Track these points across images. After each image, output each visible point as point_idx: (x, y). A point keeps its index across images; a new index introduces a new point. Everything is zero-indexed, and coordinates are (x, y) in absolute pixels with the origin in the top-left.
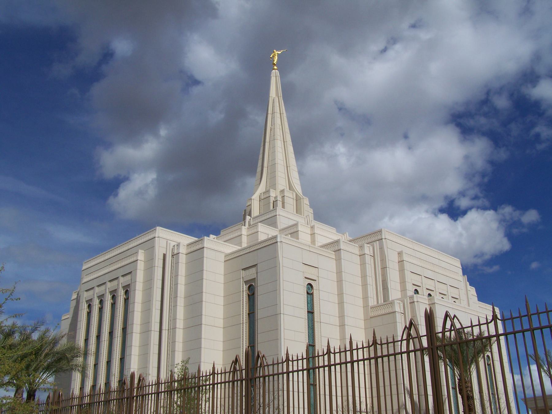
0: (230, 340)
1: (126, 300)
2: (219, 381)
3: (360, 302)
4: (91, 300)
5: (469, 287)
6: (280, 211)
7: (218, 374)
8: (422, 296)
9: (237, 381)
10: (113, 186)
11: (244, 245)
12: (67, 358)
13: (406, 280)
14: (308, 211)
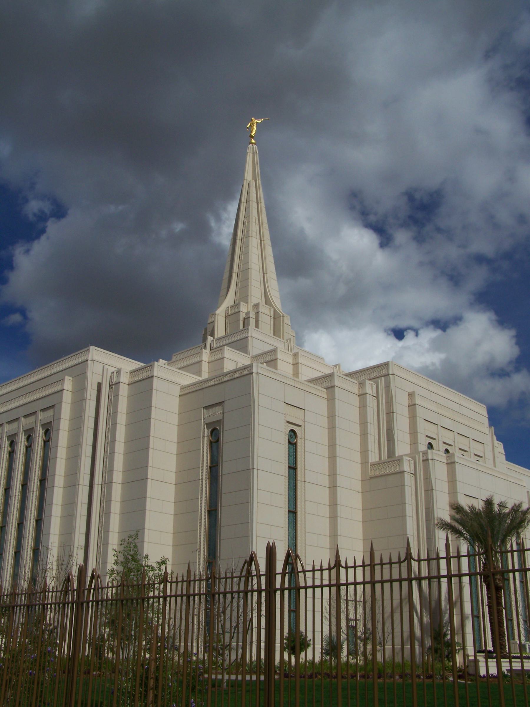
1: (46, 442)
3: (357, 457)
5: (496, 442)
6: (252, 331)
8: (438, 452)
11: (205, 375)
13: (418, 431)
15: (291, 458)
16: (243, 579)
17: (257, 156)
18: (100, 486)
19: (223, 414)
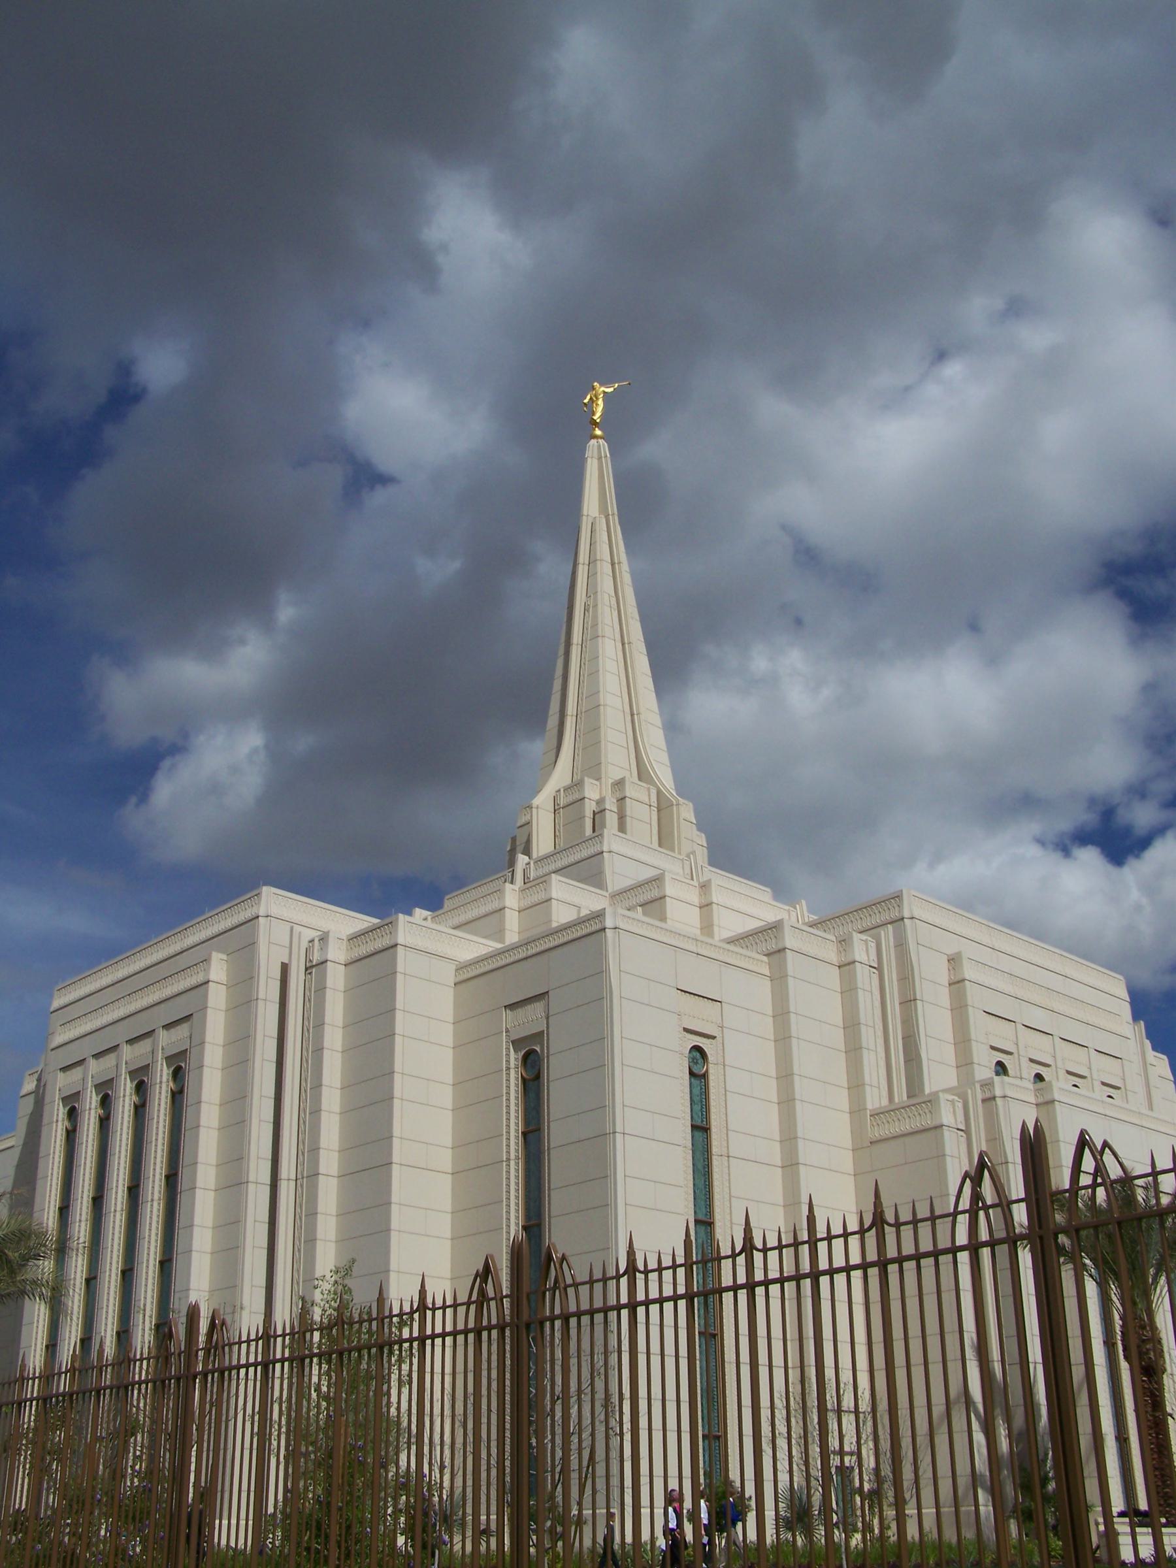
0: (471, 1209)
1: (177, 1096)
2: (438, 1330)
4: (76, 1096)
5: (1151, 1055)
6: (611, 840)
7: (434, 1309)
9: (489, 1328)
10: (139, 769)
11: (512, 936)
12: (8, 1261)
13: (973, 1037)
14: (692, 839)
15: (697, 1108)
16: (473, 1307)
18: (293, 1184)
19: (547, 1018)
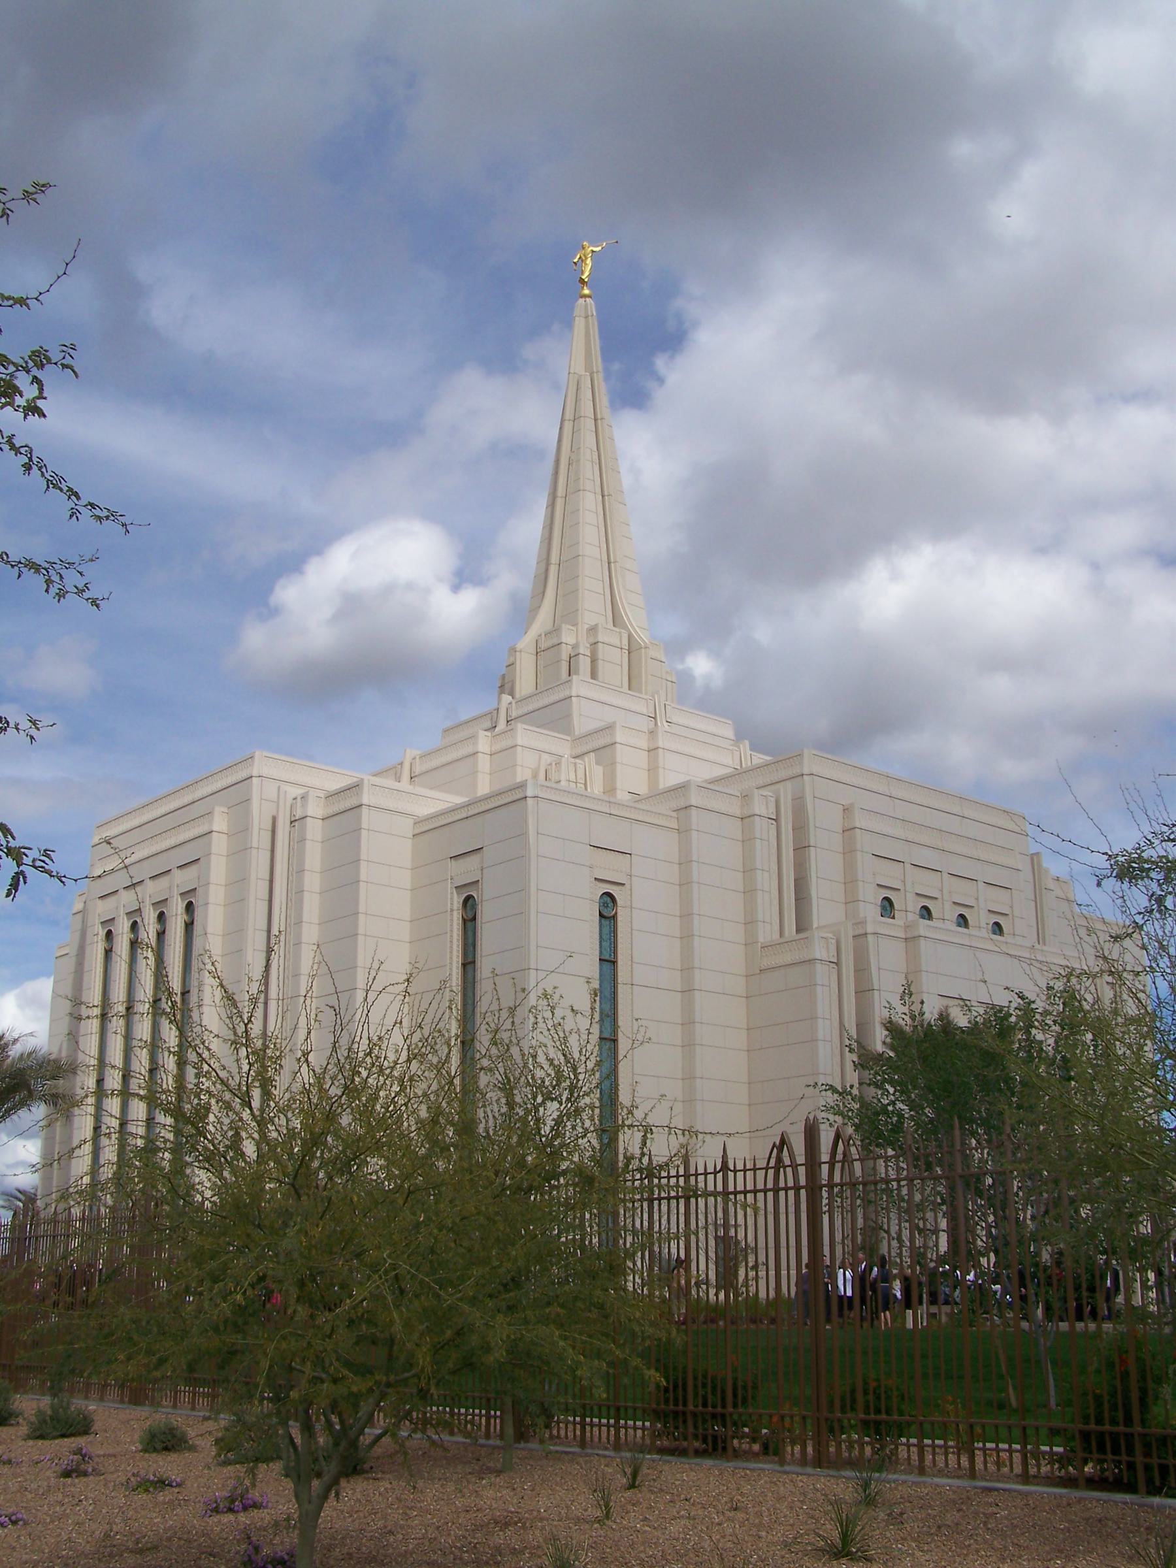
1: (189, 926)
6: (580, 686)
15: (606, 944)
16: (771, 1172)
17: (594, 324)
